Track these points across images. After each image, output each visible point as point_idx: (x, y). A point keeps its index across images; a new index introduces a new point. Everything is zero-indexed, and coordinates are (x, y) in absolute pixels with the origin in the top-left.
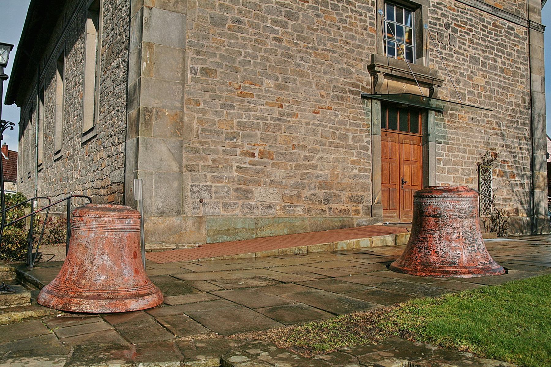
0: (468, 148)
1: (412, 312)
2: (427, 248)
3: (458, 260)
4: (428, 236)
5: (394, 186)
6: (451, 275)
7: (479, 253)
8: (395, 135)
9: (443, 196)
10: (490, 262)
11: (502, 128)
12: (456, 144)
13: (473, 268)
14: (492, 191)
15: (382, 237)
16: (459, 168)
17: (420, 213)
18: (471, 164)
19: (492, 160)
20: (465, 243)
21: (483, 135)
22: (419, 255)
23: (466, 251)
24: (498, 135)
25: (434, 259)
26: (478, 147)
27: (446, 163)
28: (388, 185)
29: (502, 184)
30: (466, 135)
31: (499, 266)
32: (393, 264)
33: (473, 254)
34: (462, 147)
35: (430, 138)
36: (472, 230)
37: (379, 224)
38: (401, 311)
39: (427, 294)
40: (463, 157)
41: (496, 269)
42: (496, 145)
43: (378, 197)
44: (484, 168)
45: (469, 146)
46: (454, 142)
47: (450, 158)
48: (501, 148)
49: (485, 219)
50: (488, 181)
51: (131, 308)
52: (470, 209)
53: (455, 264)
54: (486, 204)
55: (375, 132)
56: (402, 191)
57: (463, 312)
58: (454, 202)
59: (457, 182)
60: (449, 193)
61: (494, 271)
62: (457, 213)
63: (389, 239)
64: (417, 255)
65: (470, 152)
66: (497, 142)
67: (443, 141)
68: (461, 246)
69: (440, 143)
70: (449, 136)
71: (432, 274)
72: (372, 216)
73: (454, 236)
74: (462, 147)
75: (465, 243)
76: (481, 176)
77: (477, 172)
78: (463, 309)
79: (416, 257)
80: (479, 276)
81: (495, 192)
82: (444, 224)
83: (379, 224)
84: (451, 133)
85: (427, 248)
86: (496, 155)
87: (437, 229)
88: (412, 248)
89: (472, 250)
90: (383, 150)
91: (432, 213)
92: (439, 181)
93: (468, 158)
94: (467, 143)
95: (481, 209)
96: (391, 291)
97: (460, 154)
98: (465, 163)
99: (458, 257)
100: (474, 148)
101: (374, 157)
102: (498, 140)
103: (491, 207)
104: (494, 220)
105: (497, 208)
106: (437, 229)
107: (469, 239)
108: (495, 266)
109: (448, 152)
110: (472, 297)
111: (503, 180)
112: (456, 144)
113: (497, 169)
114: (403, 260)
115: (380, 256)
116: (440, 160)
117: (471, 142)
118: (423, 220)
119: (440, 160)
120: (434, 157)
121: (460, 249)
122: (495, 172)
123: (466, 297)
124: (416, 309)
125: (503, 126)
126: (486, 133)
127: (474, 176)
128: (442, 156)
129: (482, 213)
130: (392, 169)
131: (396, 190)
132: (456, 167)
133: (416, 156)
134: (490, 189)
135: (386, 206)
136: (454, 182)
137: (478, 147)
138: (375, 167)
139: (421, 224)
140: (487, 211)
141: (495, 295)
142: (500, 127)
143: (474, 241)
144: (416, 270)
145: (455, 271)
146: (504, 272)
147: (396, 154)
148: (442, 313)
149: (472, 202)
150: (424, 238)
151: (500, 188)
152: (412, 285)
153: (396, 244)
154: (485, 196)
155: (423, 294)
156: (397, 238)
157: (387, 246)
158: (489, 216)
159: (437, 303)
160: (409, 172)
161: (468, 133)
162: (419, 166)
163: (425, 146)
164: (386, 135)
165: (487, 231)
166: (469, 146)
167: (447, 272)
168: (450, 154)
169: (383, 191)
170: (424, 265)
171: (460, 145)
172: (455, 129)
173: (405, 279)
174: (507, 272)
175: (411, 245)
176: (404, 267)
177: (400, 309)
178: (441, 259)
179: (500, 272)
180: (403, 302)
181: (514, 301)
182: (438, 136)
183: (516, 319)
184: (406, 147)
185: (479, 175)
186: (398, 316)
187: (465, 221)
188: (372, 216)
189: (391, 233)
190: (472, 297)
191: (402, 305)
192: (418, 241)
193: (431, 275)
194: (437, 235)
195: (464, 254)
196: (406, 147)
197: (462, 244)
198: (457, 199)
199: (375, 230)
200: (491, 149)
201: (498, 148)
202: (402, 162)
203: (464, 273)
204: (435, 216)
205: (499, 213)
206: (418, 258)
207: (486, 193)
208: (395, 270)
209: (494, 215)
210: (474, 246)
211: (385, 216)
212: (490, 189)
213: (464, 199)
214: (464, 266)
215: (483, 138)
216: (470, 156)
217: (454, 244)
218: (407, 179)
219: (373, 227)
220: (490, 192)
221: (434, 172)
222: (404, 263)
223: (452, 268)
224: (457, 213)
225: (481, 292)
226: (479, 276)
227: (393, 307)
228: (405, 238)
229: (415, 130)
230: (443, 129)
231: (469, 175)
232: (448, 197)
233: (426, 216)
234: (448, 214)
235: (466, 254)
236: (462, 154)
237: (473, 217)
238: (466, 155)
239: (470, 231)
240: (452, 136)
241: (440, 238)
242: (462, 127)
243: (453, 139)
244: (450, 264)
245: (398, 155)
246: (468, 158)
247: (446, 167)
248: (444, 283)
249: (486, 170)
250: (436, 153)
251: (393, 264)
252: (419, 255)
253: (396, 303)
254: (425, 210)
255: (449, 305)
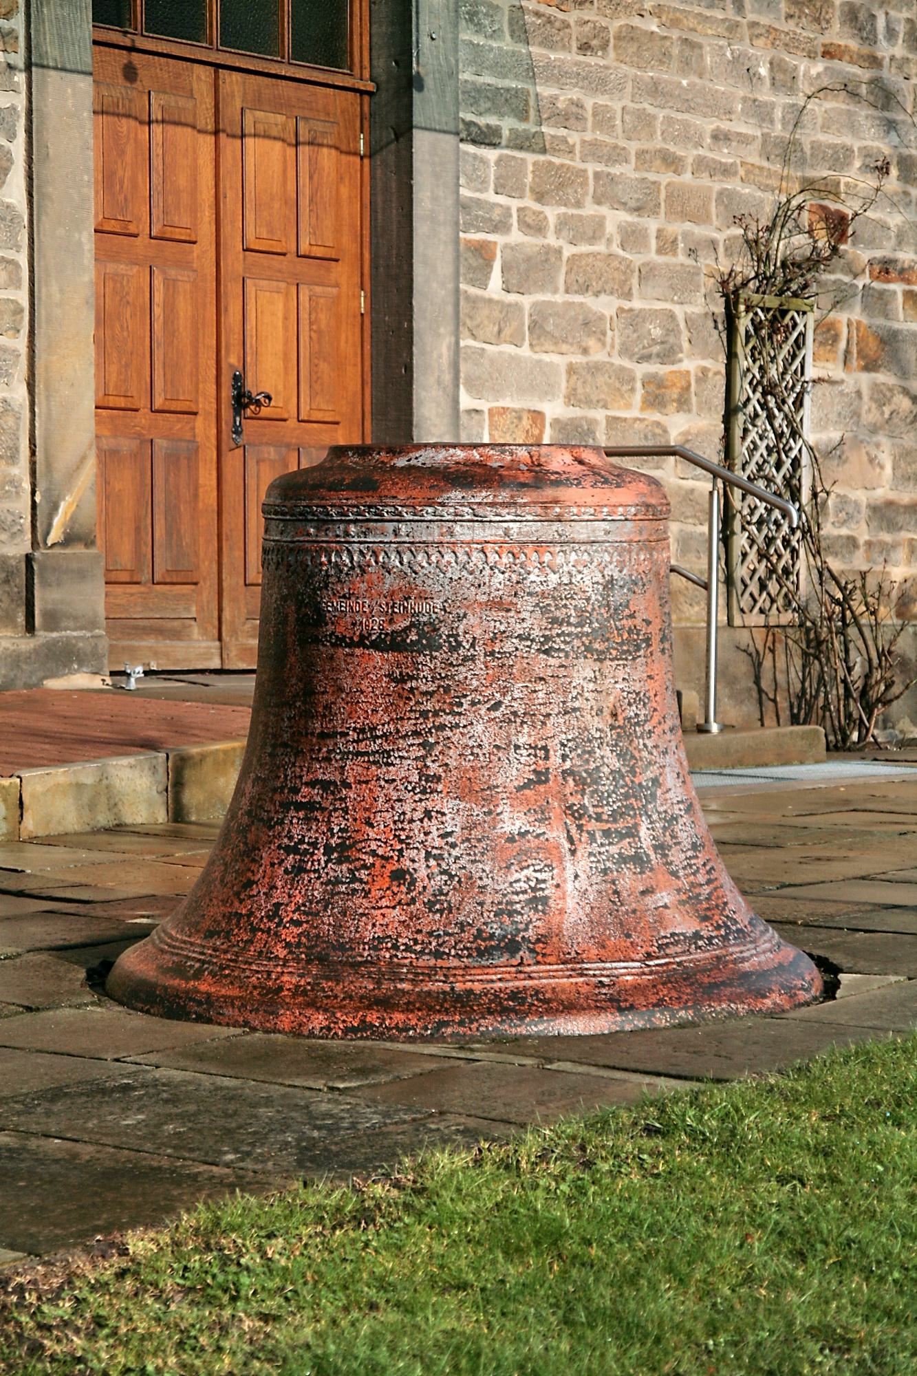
0: (665, 177)
1: (198, 1293)
2: (343, 851)
3: (532, 924)
4: (353, 769)
5: (178, 424)
6: (489, 1024)
7: (663, 877)
8: (188, 82)
9: (447, 513)
10: (730, 932)
11: (885, 50)
12: (592, 150)
13: (627, 972)
14: (805, 460)
15: (85, 772)
16: (606, 305)
17: (302, 622)
18: (682, 283)
19: (814, 262)
20: (577, 814)
21: (765, 95)
22: (290, 897)
23: (583, 864)
24: (854, 95)
25: (383, 919)
26: (726, 171)
27: (528, 271)
28: (143, 418)
29: (870, 414)
30: (654, 90)
31: (790, 953)
32: (132, 961)
33: (628, 880)
34: (626, 170)
35: (424, 106)
36: (623, 729)
37: (81, 680)
38: (129, 1284)
39: (314, 1159)
40: (632, 237)
41: (763, 974)
42: (840, 158)
43: (75, 502)
44: (762, 308)
45: (672, 162)
46: (574, 138)
47: (552, 240)
48: (869, 182)
49: (759, 636)
50: (780, 396)
51: (697, 704)
52: (617, 597)
53: (512, 947)
54: (770, 541)
55: (50, 50)
56: (233, 461)
57: (513, 1272)
58: (516, 548)
59: (588, 403)
60: (483, 495)
61: (751, 985)
62: (533, 623)
63: (136, 785)
64: (279, 896)
65: (683, 205)
66: (847, 140)
67: (507, 125)
68: (556, 834)
69: (486, 138)
70: (545, 91)
71: (373, 1017)
72: (30, 627)
73: (514, 771)
74: (626, 170)
75: (577, 814)
76: (744, 363)
77: (716, 339)
78: (513, 1252)
79: (275, 913)
80: (661, 1019)
81: (831, 469)
82: (450, 695)
83: (81, 680)
84: (559, 76)
85: (342, 847)
86: (838, 226)
87: (407, 727)
88: (250, 853)
89: (623, 859)
90: (107, 179)
91: (376, 624)
92: (476, 388)
93: (667, 245)
94: (658, 143)
95: (741, 572)
96: (86, 1151)
97: (615, 219)
98: (647, 274)
99: (538, 902)
100: (705, 181)
101: (45, 226)
102: (854, 129)
103: (801, 565)
104: (814, 648)
105: (835, 564)
106: (407, 727)
107: (606, 786)
108: (764, 951)
109: (540, 197)
110: (588, 1165)
111: (875, 387)
112: (592, 150)
113: (841, 318)
114: (195, 928)
115: (56, 902)
116: (483, 252)
117: (688, 136)
118: (325, 664)
119: (483, 252)
120: (445, 233)
121: (549, 849)
122: (828, 333)
123: (554, 1168)
124: (225, 1261)
125: (891, 33)
126: (783, 78)
127: (700, 363)
128: (501, 226)
129: (746, 602)
130: (170, 307)
131: (195, 452)
132: (588, 300)
133: (328, 222)
134: (796, 446)
135: (126, 558)
136: (572, 398)
137: (726, 171)
138: (49, 291)
139: (309, 692)
140: (773, 587)
141: (728, 1146)
142: (870, 38)
143: (636, 797)
144: (270, 999)
145: (514, 995)
146: (816, 991)
147: (194, 210)
148: (382, 1284)
149: (624, 548)
150: (325, 785)
151: (857, 443)
152: (231, 1097)
153: (178, 812)
154: (763, 493)
155: (289, 1160)
156: (188, 774)
157: (118, 829)
158: (788, 617)
159: (364, 1216)
160: (291, 341)
161: (667, 75)
162: (347, 293)
163: (389, 155)
164: (130, 73)
165: (770, 720)
166: (672, 162)
167: (464, 1003)
168: (552, 213)
169: (108, 458)
170: (322, 960)
171: (616, 155)
172: (585, 48)
173: (198, 1056)
174: (830, 990)
175: (244, 831)
176: (198, 975)
177: (121, 1275)
178: (431, 921)
179: (790, 992)
180: (151, 1217)
181: (834, 1180)
182: (477, 95)
183: (823, 1300)
184: (265, 160)
185: (731, 356)
186: (99, 1322)
187: (584, 670)
188: (30, 627)
189: (149, 745)
190: (588, 1165)
191: (139, 1243)
192: (286, 806)
193: (365, 1026)
194: (405, 769)
195: (572, 888)
196: (265, 160)
197: (566, 811)
198: (534, 529)
199: (46, 724)
200: (808, 186)
201: (855, 178)
202: (234, 261)
203: (570, 1007)
204: (393, 643)
205: (845, 603)
206: (289, 914)
207: (770, 470)
208: (142, 997)
209: (815, 611)
210: (632, 833)
211: (119, 624)
212: (796, 446)
213: (581, 531)
214: (573, 961)
215: (761, 112)
216: (677, 228)
217: (512, 821)
218: (269, 375)
219: (37, 701)
220: (796, 463)
221: (446, 330)
222: (196, 948)
223: (497, 977)
224: (533, 623)
225: (650, 1131)
226: (661, 1019)
227: (80, 1262)
228: (219, 787)
229: (325, 45)
230: (506, 44)
231: (668, 355)
232: (479, 520)
233: (340, 642)
234: (475, 625)
235: (583, 883)
236: (624, 217)
237: (633, 645)
238: (652, 225)
239: (610, 736)
240: (565, 96)
241: (428, 783)
242: (629, 35)
243: (571, 117)
244: (487, 948)
245: (207, 215)
246: (667, 245)
247: (526, 301)
248: (440, 1077)
249: (776, 323)
250: (463, 206)
251: (132, 961)
252: (290, 897)
253: (106, 1229)
254: (332, 605)
255: (438, 1226)
